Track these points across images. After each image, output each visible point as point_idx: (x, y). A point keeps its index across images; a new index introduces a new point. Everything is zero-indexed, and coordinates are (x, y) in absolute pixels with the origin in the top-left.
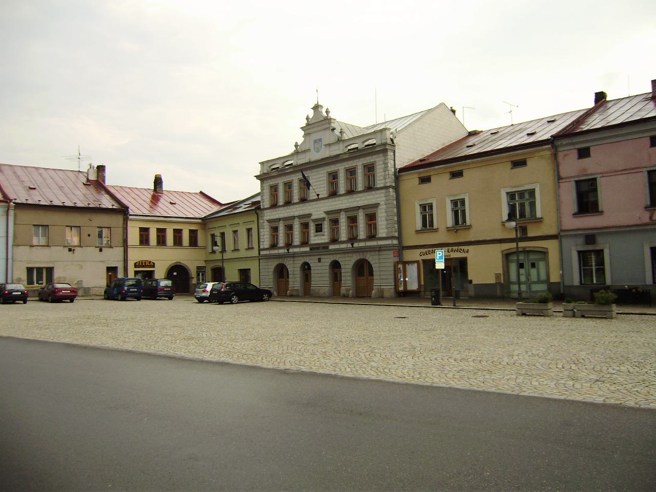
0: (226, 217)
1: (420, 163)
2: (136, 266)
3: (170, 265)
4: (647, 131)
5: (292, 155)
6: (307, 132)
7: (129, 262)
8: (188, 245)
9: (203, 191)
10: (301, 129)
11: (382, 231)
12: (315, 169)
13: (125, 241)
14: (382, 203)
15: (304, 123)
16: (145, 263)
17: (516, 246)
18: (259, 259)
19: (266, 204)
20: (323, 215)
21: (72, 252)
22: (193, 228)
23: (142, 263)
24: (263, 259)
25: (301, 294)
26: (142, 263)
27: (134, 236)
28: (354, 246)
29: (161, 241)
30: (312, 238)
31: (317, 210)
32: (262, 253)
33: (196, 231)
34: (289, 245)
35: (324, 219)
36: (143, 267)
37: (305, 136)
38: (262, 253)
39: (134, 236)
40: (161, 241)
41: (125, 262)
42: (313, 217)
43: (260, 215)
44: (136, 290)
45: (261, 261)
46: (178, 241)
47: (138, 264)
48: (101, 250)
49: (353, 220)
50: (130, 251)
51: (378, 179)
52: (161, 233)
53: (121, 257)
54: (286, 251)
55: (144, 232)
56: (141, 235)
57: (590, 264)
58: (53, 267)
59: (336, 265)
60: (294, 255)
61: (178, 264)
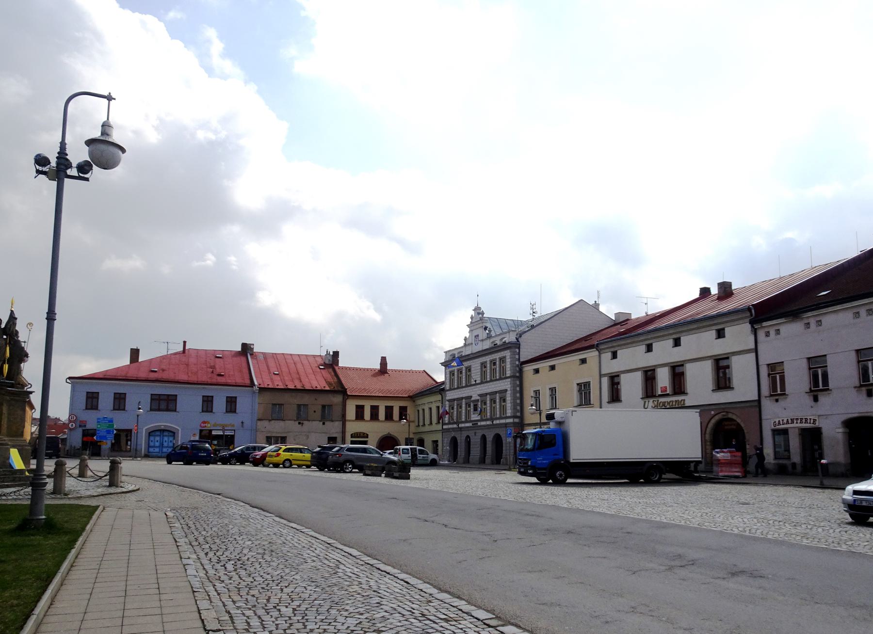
0: (398, 399)
1: (547, 355)
2: (352, 436)
3: (382, 437)
4: (671, 334)
5: (462, 347)
6: (472, 328)
7: (346, 433)
8: (354, 418)
9: (426, 370)
10: (467, 327)
11: (509, 412)
12: (487, 355)
13: (344, 416)
14: (509, 389)
15: (469, 321)
16: (360, 435)
17: (150, 449)
18: (442, 433)
19: (447, 387)
20: (478, 398)
21: (301, 425)
22: (403, 404)
23: (357, 434)
24: (445, 432)
25: (799, 468)
26: (357, 434)
27: (351, 413)
28: (494, 422)
29: (374, 416)
30: (472, 416)
31: (475, 392)
32: (445, 427)
33: (406, 407)
34: (424, 425)
35: (478, 400)
36: (358, 437)
37: (471, 331)
38: (445, 427)
39: (351, 413)
40: (374, 416)
41: (343, 434)
42: (473, 399)
43: (443, 395)
44: (205, 454)
45: (443, 434)
46: (389, 417)
47: (353, 435)
48: (324, 424)
49: (493, 401)
50: (348, 424)
51: (480, 373)
52: (375, 410)
53: (340, 429)
54: (491, 423)
55: (360, 410)
56: (357, 412)
57: (795, 443)
58: (286, 437)
59: (484, 438)
60: (461, 429)
61: (389, 435)
